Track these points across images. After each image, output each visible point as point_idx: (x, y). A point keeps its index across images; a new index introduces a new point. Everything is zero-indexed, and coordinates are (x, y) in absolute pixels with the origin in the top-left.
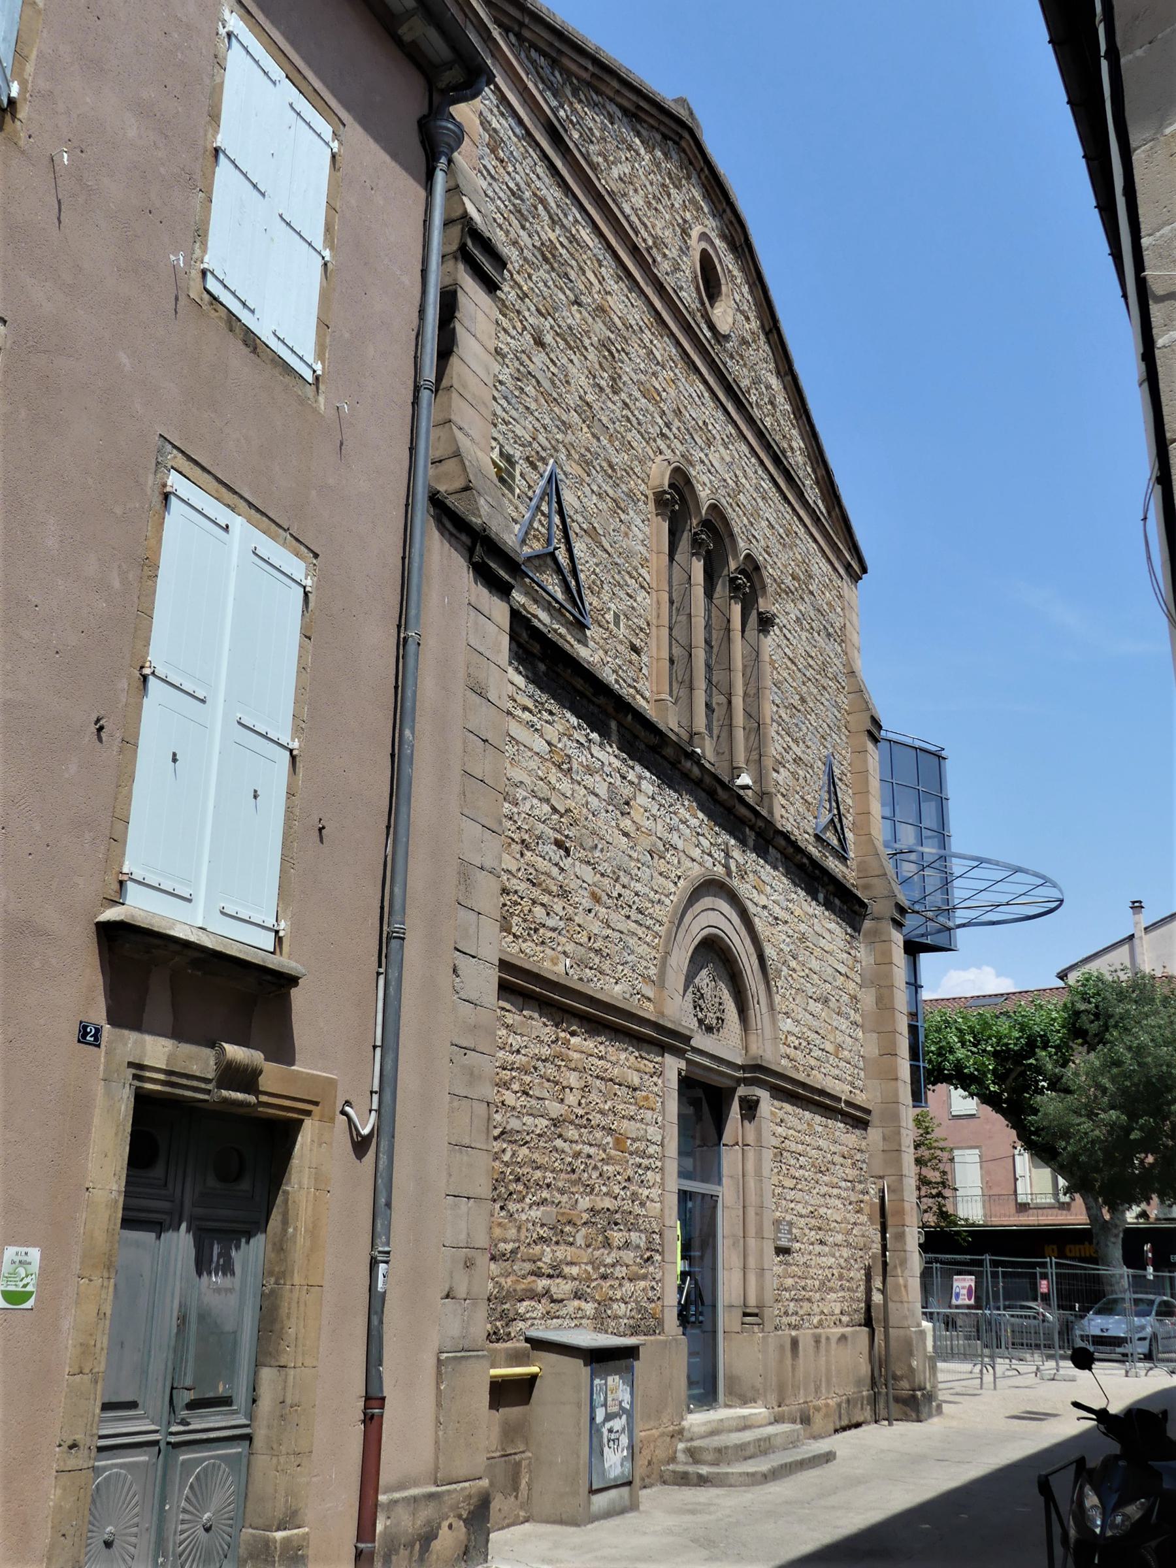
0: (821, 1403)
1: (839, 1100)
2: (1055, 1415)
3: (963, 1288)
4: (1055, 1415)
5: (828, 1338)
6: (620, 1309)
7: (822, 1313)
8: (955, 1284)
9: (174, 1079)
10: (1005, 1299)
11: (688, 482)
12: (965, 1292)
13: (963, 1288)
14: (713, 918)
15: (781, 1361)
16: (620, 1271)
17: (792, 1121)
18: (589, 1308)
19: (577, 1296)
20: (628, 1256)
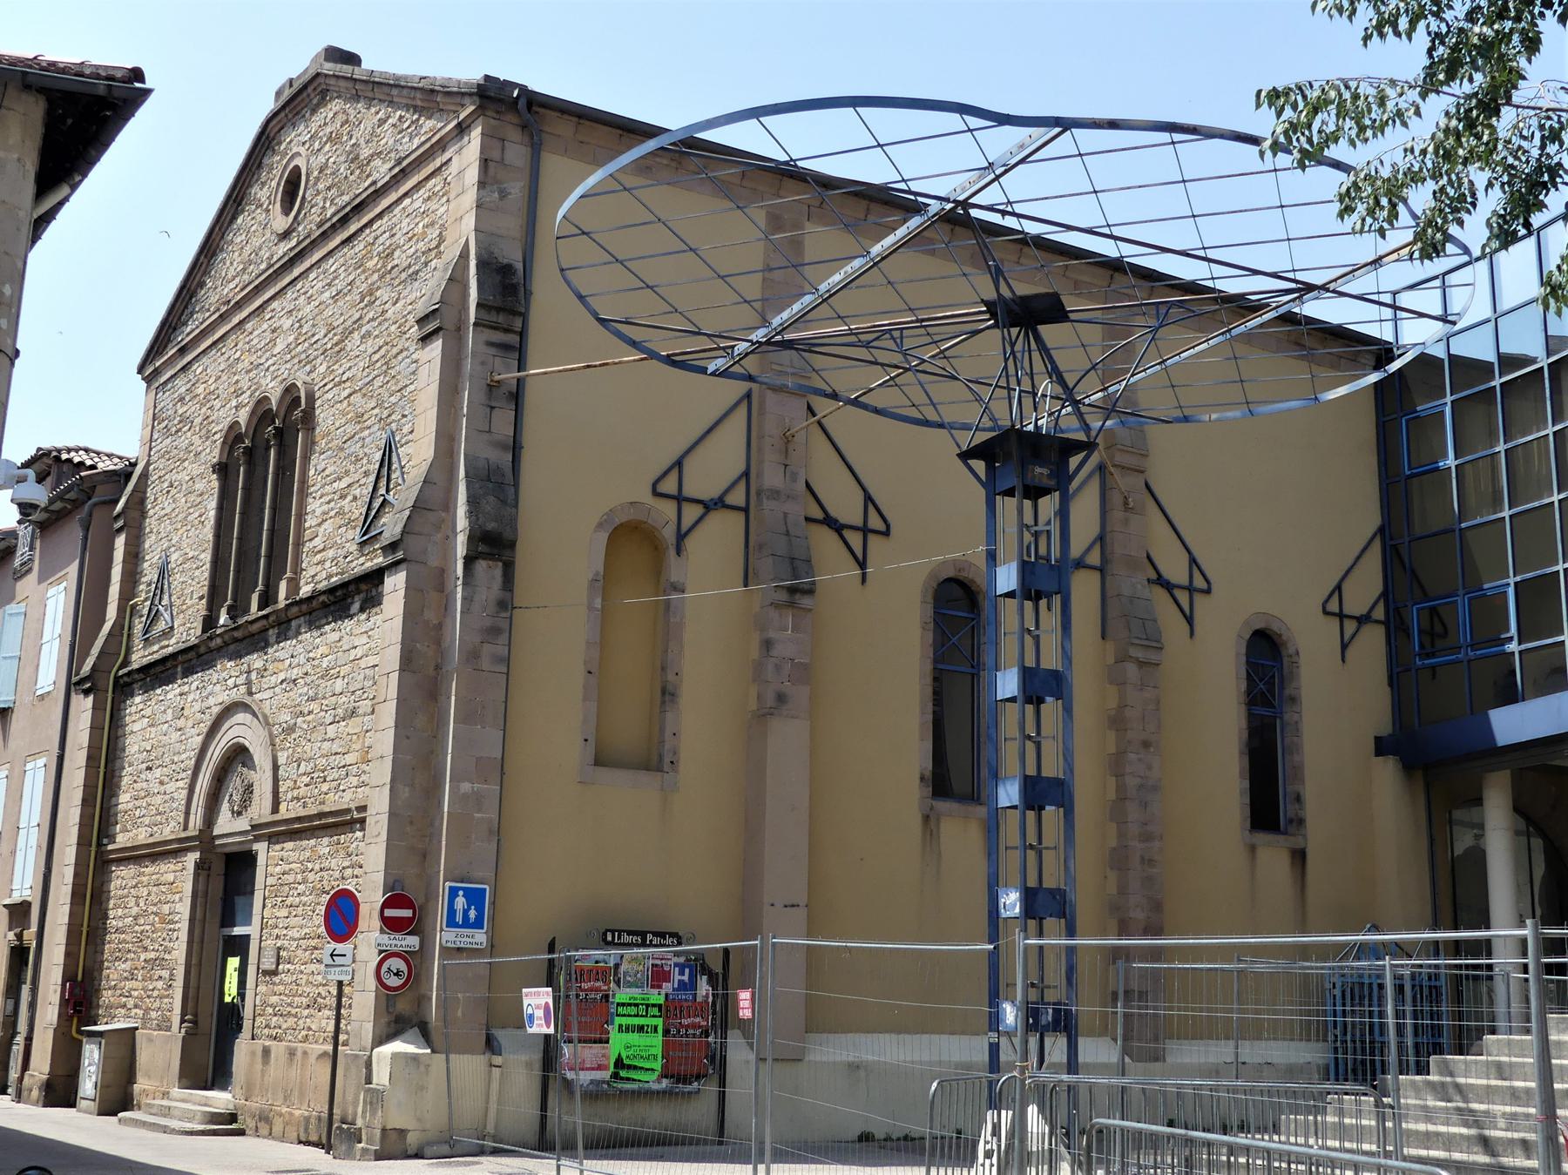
0: (285, 1110)
1: (348, 811)
2: (1192, 634)
3: (538, 1007)
4: (1192, 634)
5: (305, 1053)
6: (153, 1014)
7: (310, 1029)
8: (526, 1002)
9: (1341, 1071)
10: (580, 1030)
11: (309, 418)
12: (540, 1013)
13: (538, 1007)
14: (248, 733)
15: (251, 1065)
16: (156, 993)
17: (293, 856)
18: (140, 1012)
19: (136, 1006)
20: (160, 984)
